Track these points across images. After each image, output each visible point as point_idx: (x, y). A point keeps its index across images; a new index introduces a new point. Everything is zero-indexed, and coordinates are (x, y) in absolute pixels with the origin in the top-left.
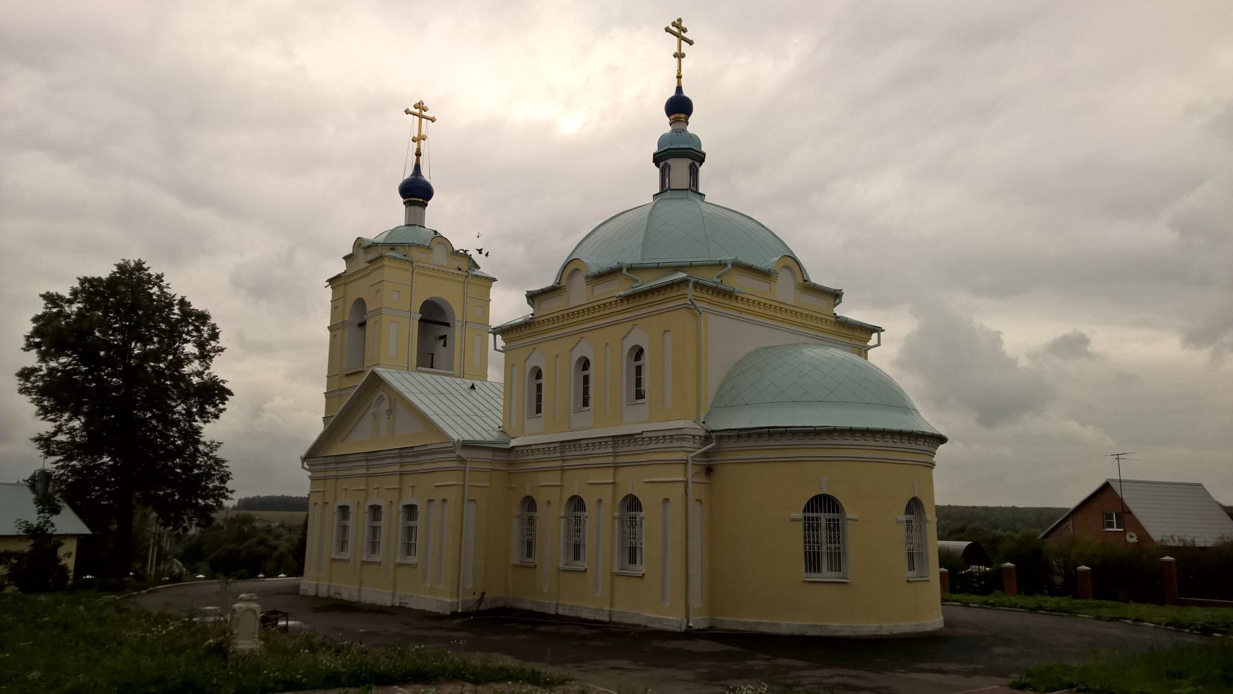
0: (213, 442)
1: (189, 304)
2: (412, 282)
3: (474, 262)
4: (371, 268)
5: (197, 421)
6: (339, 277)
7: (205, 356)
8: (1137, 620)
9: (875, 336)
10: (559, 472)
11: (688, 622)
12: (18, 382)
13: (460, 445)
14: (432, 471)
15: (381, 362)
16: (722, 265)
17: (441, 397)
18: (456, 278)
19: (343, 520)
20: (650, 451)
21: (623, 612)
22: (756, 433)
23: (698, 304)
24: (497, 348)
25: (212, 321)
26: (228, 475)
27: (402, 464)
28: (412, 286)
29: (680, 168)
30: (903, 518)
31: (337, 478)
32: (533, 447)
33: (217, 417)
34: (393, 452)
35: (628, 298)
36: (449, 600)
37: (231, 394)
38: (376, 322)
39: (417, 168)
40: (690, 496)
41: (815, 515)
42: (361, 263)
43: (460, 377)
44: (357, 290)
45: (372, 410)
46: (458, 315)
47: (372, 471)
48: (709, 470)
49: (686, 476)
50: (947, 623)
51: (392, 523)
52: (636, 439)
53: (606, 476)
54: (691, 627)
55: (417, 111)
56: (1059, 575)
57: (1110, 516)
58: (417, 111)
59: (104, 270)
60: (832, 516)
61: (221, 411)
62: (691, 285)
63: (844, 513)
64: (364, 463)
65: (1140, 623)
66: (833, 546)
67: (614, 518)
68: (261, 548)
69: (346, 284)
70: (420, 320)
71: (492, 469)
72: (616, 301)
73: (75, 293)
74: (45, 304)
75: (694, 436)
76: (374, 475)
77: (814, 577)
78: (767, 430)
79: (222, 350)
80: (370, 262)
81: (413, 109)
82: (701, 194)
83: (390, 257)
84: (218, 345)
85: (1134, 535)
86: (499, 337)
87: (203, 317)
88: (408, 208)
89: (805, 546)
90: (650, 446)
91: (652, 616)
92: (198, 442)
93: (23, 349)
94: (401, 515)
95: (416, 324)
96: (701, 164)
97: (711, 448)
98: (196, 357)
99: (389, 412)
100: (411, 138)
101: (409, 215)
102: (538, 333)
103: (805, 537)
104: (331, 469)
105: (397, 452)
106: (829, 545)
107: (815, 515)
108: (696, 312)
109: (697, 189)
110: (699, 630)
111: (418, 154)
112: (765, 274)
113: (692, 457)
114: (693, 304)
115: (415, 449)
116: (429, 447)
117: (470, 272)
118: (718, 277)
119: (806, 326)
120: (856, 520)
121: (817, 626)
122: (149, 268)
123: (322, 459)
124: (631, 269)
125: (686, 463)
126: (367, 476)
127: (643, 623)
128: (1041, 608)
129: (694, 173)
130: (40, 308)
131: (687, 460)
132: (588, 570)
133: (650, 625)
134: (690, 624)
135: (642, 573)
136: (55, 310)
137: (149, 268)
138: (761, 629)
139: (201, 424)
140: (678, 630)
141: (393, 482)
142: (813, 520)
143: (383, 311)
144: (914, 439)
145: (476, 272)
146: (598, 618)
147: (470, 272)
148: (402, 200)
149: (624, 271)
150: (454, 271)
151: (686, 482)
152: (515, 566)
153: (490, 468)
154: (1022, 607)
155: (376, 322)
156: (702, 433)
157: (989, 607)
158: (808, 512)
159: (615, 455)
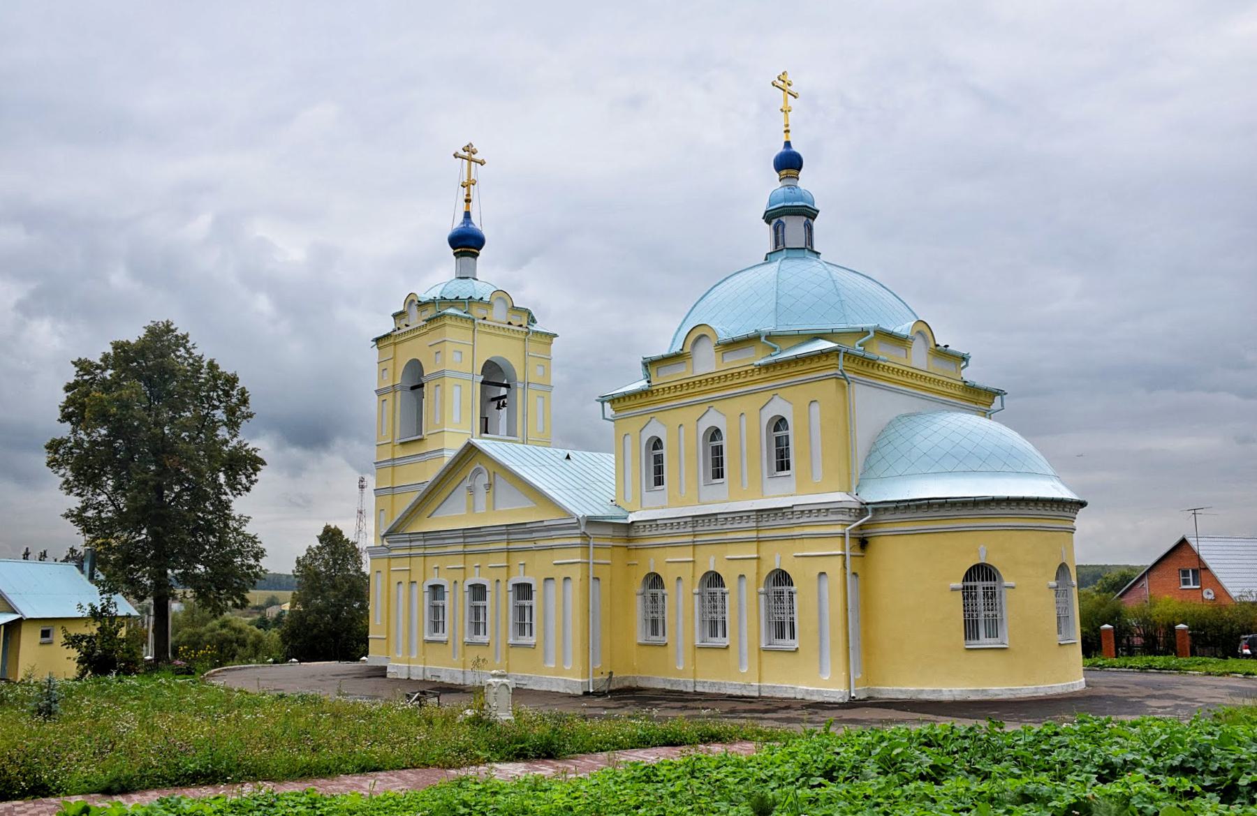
0: (242, 516)
1: (217, 367)
2: (474, 341)
3: (533, 317)
4: (428, 327)
5: (226, 494)
6: (387, 336)
7: (233, 425)
8: (1248, 674)
9: (998, 399)
10: (691, 548)
11: (850, 692)
12: (47, 455)
13: (585, 521)
14: (551, 548)
15: (446, 429)
16: (864, 332)
17: (543, 469)
18: (517, 336)
19: (435, 598)
20: (799, 525)
21: (774, 687)
22: (936, 504)
23: (847, 374)
24: (606, 417)
25: (240, 384)
26: (262, 552)
27: (509, 542)
28: (473, 345)
29: (794, 227)
30: (1054, 584)
31: (425, 556)
32: (658, 522)
33: (248, 490)
34: (518, 527)
35: (767, 367)
36: (580, 680)
37: (264, 463)
38: (437, 386)
39: (467, 215)
40: (848, 571)
41: (973, 584)
42: (416, 319)
43: (523, 443)
44: (406, 353)
45: (467, 483)
46: (520, 377)
47: (469, 548)
48: (863, 543)
49: (844, 549)
50: (1088, 684)
51: (500, 605)
52: (784, 513)
53: (750, 551)
54: (854, 697)
55: (466, 154)
56: (1139, 635)
57: (1185, 573)
58: (466, 154)
59: (133, 334)
60: (986, 584)
61: (252, 482)
62: (841, 355)
63: (1001, 580)
64: (462, 540)
65: (1251, 677)
66: (991, 613)
67: (760, 593)
68: (224, 631)
69: (395, 344)
70: (482, 383)
71: (613, 546)
72: (753, 370)
73: (106, 358)
74: (77, 372)
75: (850, 509)
76: (472, 553)
77: (974, 644)
78: (926, 501)
79: (251, 416)
80: (429, 320)
81: (462, 153)
82: (817, 253)
83: (451, 316)
84: (249, 411)
85: (1211, 592)
86: (607, 405)
87: (232, 381)
88: (459, 260)
89: (965, 615)
90: (801, 520)
91: (810, 689)
92: (229, 517)
93: (59, 420)
94: (467, 594)
95: (479, 385)
96: (814, 220)
97: (867, 521)
98: (225, 424)
99: (489, 486)
100: (461, 184)
101: (460, 267)
102: (655, 402)
103: (964, 605)
104: (418, 547)
105: (504, 528)
106: (987, 613)
107: (973, 584)
108: (845, 382)
109: (812, 247)
110: (859, 700)
111: (468, 201)
112: (899, 340)
113: (849, 530)
114: (843, 375)
115: (528, 526)
116: (545, 524)
117: (531, 328)
118: (860, 345)
119: (939, 392)
120: (1013, 588)
121: (978, 690)
122: (176, 329)
123: (407, 536)
124: (769, 337)
125: (843, 536)
126: (465, 553)
127: (799, 696)
128: (1150, 667)
129: (809, 229)
130: (71, 375)
131: (844, 534)
132: (800, 649)
133: (808, 698)
134: (853, 695)
135: (796, 647)
136: (86, 377)
137: (176, 329)
138: (924, 697)
139: (231, 497)
140: (841, 701)
141: (501, 560)
142: (971, 589)
143: (447, 374)
144: (1024, 504)
145: (536, 328)
146: (746, 693)
147: (531, 328)
148: (452, 251)
149: (763, 339)
150: (504, 326)
151: (844, 555)
152: (640, 645)
153: (612, 543)
154: (1131, 667)
155: (437, 386)
156: (857, 506)
157: (1098, 669)
158: (967, 581)
159: (758, 529)
